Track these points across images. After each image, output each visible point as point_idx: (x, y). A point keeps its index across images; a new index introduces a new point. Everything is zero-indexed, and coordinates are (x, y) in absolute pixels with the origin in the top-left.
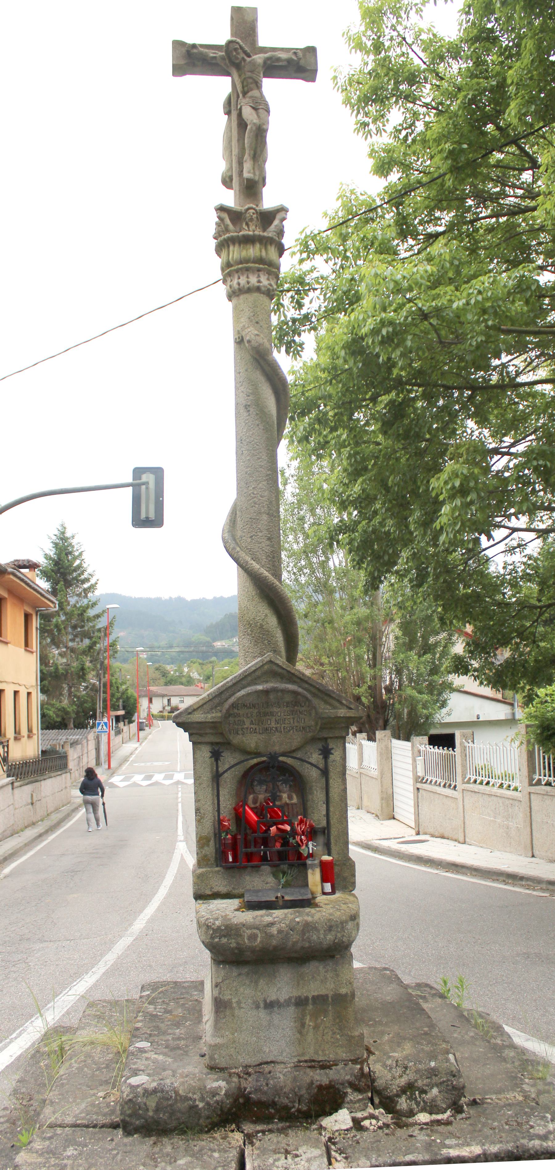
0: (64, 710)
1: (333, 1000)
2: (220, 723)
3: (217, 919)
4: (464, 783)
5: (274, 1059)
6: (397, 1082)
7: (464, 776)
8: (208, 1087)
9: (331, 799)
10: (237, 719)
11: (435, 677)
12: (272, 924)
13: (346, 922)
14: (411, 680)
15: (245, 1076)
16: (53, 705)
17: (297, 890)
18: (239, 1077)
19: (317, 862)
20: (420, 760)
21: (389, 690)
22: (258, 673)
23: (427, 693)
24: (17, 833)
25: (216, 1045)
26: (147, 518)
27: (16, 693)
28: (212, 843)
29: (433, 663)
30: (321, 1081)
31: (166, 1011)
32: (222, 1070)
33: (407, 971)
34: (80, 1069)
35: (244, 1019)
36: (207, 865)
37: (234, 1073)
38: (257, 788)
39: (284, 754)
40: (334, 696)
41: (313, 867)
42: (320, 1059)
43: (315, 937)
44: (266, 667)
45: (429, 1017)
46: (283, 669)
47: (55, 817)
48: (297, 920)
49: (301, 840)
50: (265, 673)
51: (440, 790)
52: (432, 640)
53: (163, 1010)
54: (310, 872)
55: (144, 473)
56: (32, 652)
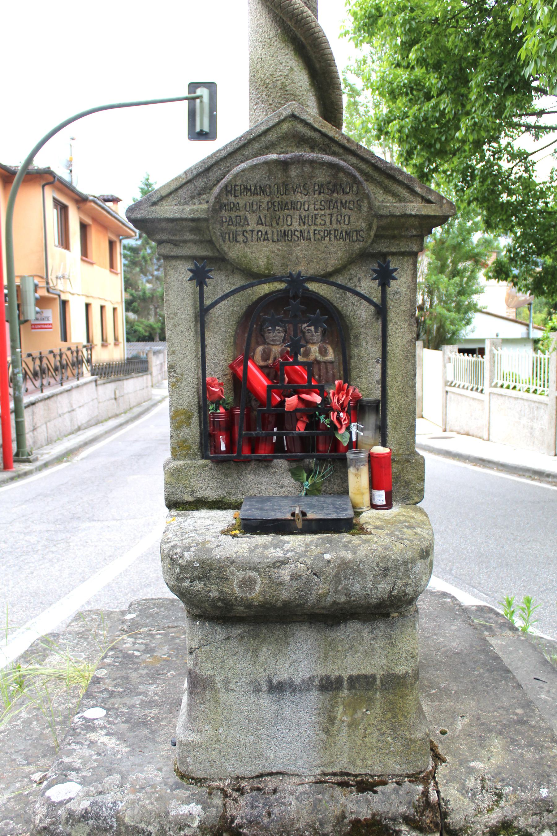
0: (151, 327)
1: (382, 684)
2: (206, 220)
3: (188, 549)
4: (491, 386)
5: (282, 770)
6: (485, 818)
7: (491, 381)
8: (172, 813)
9: (390, 356)
10: (233, 214)
11: (463, 298)
12: (282, 563)
13: (413, 561)
14: (440, 301)
15: (236, 795)
16: (142, 323)
17: (329, 500)
18: (226, 796)
19: (364, 456)
20: (450, 366)
21: (421, 308)
22: (272, 137)
23: (455, 312)
24: (102, 422)
25: (188, 744)
26: (201, 131)
27: (102, 308)
28: (195, 421)
29: (461, 285)
30: (358, 813)
31: (149, 650)
32: (199, 781)
33: (448, 568)
34: (27, 723)
35: (234, 708)
36: (186, 456)
37: (218, 788)
38: (270, 336)
39: (312, 279)
40: (401, 178)
41: (357, 463)
42: (358, 772)
43: (357, 587)
44: (285, 127)
45: (519, 686)
46: (315, 130)
47: (137, 411)
48: (327, 556)
49: (339, 419)
50: (284, 138)
51: (468, 393)
52: (460, 266)
53: (143, 647)
54: (351, 471)
55: (199, 87)
56: (117, 274)
